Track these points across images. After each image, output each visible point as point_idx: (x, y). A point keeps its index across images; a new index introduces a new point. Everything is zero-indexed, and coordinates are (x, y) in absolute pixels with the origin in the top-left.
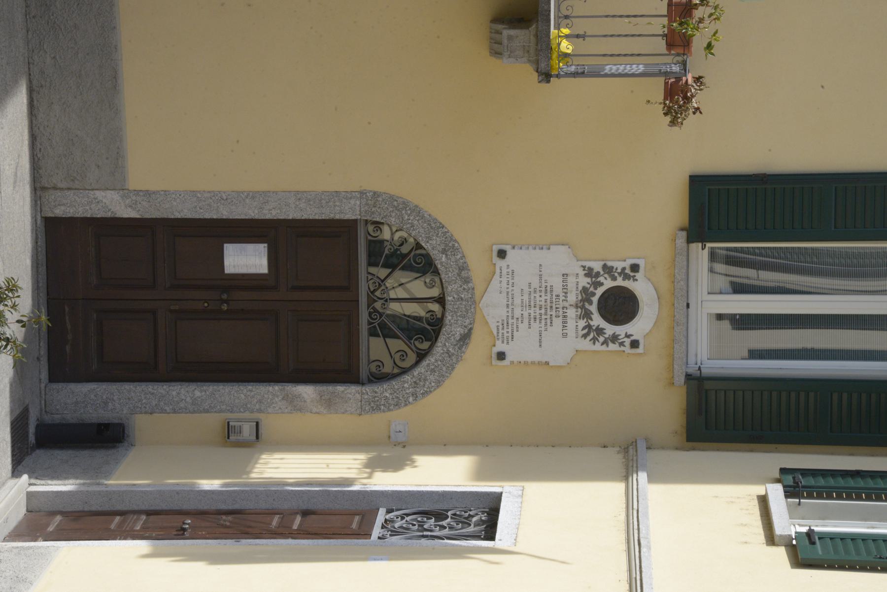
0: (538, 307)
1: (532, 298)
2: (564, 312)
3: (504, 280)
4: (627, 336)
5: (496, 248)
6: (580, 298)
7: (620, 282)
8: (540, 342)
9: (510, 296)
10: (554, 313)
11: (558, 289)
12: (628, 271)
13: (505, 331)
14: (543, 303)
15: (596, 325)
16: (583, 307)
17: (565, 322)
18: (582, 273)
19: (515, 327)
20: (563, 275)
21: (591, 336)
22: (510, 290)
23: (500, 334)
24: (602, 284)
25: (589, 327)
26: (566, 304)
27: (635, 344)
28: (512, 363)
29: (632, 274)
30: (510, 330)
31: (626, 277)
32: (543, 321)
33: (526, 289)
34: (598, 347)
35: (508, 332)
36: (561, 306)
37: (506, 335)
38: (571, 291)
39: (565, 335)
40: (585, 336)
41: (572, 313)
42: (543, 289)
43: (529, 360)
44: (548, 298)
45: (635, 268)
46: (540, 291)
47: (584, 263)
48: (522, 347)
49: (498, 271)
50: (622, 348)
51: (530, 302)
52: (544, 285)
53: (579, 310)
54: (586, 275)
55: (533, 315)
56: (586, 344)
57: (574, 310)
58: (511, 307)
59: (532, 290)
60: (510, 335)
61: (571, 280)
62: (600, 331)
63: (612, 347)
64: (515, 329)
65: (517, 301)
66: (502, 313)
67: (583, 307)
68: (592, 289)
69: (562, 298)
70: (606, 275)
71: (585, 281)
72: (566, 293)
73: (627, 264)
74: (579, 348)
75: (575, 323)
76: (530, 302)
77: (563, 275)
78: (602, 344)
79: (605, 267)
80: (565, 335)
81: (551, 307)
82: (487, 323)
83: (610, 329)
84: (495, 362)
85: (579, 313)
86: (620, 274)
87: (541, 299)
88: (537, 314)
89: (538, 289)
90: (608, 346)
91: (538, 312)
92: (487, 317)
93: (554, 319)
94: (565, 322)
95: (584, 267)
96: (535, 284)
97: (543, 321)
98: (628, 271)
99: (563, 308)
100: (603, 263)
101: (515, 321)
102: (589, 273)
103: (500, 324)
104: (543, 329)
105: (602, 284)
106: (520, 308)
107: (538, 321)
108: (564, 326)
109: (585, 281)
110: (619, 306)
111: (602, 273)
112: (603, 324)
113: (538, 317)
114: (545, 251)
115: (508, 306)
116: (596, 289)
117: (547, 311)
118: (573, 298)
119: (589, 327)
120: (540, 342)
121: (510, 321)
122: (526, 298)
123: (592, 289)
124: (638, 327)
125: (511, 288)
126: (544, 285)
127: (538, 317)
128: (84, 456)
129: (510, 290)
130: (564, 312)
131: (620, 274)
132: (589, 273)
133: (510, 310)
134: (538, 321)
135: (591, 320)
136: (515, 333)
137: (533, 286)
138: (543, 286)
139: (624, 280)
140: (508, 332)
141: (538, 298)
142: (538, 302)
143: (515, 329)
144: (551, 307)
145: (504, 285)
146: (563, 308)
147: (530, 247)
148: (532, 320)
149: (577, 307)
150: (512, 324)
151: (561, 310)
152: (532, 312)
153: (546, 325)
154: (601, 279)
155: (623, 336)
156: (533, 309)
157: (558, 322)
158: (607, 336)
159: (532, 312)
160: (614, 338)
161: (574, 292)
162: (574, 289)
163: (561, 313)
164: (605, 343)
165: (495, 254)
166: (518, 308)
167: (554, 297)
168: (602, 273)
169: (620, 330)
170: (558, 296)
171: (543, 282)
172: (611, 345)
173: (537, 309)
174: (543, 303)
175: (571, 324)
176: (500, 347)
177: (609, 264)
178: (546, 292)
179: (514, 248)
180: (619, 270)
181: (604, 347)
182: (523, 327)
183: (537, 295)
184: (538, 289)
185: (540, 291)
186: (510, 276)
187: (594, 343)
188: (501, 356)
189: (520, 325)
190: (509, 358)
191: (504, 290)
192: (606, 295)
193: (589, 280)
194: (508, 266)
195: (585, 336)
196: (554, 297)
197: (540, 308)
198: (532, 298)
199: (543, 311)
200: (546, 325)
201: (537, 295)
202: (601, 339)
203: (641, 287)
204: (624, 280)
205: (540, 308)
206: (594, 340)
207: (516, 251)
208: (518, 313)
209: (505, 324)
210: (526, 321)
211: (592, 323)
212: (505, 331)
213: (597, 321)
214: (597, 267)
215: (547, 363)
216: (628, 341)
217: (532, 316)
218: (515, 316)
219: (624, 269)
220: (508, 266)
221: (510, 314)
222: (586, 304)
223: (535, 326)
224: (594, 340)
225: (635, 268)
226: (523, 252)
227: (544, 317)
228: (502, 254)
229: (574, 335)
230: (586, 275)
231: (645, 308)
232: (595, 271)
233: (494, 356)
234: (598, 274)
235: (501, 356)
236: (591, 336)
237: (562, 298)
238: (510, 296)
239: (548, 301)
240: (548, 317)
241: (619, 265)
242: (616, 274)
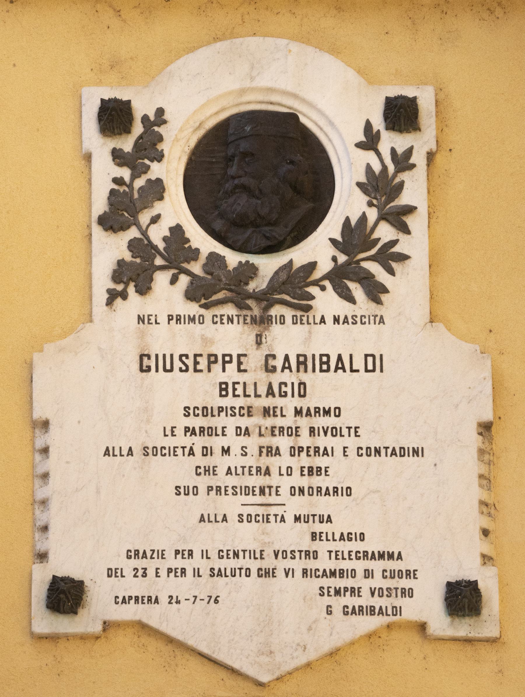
0: (265, 461)
1: (232, 481)
2: (286, 366)
3: (167, 586)
4: (370, 141)
5: (45, 622)
6: (230, 310)
7: (171, 170)
8: (403, 452)
9: (230, 564)
10: (290, 404)
11: (201, 388)
12: (127, 144)
13: (366, 585)
14: (253, 443)
15: (332, 251)
16: (266, 298)
17: (324, 364)
18: (134, 303)
19: (346, 547)
20: (144, 369)
21: (375, 268)
22: (204, 566)
23: (377, 602)
24: (177, 231)
25: (339, 277)
26: (255, 359)
27: (401, 114)
28: (486, 559)
29: (138, 129)
30: (360, 566)
31: (149, 147)
32: (322, 441)
33: (201, 504)
34: (415, 244)
35: (368, 574)
36: (264, 379)
37: (378, 582)
38: (206, 341)
39: (374, 363)
40: (376, 291)
41: (287, 337)
42: (199, 442)
43: (476, 493)
44: (231, 423)
45: (114, 116)
46: (206, 451)
47: (100, 296)
48: (426, 520)
49: (130, 612)
50: (418, 158)
51: (248, 491)
52: (182, 440)
53: (276, 311)
54: (144, 290)
55: (297, 480)
56: (407, 286)
57: (276, 329)
58: (269, 562)
59: (203, 482)
60: (377, 566)
61: (165, 340)
62: (354, 238)
63: (414, 190)
64: (355, 546)
65: (246, 536)
66: (293, 598)
67: (266, 298)
68: (196, 268)
69: (231, 374)
70: (144, 218)
71: (167, 294)
72: (212, 359)
73: (100, 147)
74: (420, 310)
75: (330, 324)
76: (248, 491)
77: (144, 369)
78: (405, 229)
79: (111, 222)
80: (374, 363)
81: (266, 412)
82: (333, 654)
83: (348, 202)
84: (487, 626)
85: (288, 313)
86: (138, 171)
87: (238, 449)
88: (295, 463)
89: (199, 460)
90: (410, 210)
91: (285, 460)
92: (312, 655)
93: (310, 402)
94: (324, 364)
95: (113, 296)
96: (181, 470)
97: (322, 441)
98: (127, 144)
99: (270, 370)
100: (97, 231)
101: (322, 547)
102: (134, 276)
103: (338, 603)
104: (352, 442)
105: (177, 231)
106: (273, 526)
107: (321, 462)
108: (340, 366)
109: (167, 294)
110: (261, 177)
111: (133, 233)
112: (331, 227)
113: (305, 461)
114: (54, 438)
115: (266, 573)
116: (195, 254)
117: (284, 432)
118: (230, 335)
119: (339, 277)
120: (403, 452)
121: (324, 563)
122: (232, 505)
123: (196, 268)
124: (336, 107)
125: (197, 561)
126: (182, 440)
127: (305, 461)
128: (468, 638)
129: (204, 566)
130: (286, 366)
131: (138, 171)
132: (134, 276)
133: (282, 564)
134: (321, 462)
135: (312, 266)
136: (371, 545)
137: (189, 480)
138: (188, 441)
139: (159, 157)
140: (368, 574)
141: (235, 460)
142: (250, 461)
143: (355, 546)
144: (266, 412)
145: (183, 587)
146: (270, 370)
147: (42, 518)
148: (317, 481)
149: (264, 321)
150: (337, 555)
151: (276, 379)
152: (286, 483)
153: (335, 432)
154: (157, 235)
155: (370, 157)
156: (274, 480)
157: (323, 389)
158: (372, 215)
159: (286, 483)
160: (380, 187)
161: (208, 329)
162: (196, 328)
163: (287, 377)
164: (399, 218)
165: (63, 624)
166: (262, 396)
167: (228, 402)
168: (133, 233)
169: (349, 167)
170: (223, 389)
171: (169, 442)
172: (405, 199)
173: (274, 462)
174: (253, 443)
175: (328, 340)
176: (427, 604)
177: (100, 205)
178: (211, 431)
179: (42, 557)
180: (125, 173)
181: (417, 223)
182: (344, 516)
183: (222, 463)
184: (199, 460)
185: (206, 451)
186: (151, 565)
187: (403, 258)
188: (462, 598)
189: (338, 527)
190: (470, 570)
191: (206, 586)
192: (218, 225)
193: (162, 279)
194: (111, 573)
195: (376, 291)
196: (228, 402)
197: (273, 451)
198: (232, 481)
199: (284, 443)
200: (335, 432)
201: (222, 463)
202: (385, 232)
203: (193, 95)
204: (159, 157)
205: (273, 451)
206: (389, 257)
207: (53, 543)
208: (294, 536)
209: (335, 583)
210: (323, 505)
211: (325, 266)
212: (366, 585)
213: (318, 249)
214: (112, 249)
215: (485, 428)
216: (389, 141)
217: (305, 482)
218: (306, 544)
219: (117, 156)
220: (111, 573)
221: (298, 565)
222: (252, 286)
223: (340, 470)
224: (389, 257)
225: (114, 116)
226: (55, 517)
227: (305, 440)
228: (65, 596)
229: (372, 328)
230: (144, 290)
231: (263, 82)
232: (127, 256)
233: (464, 628)
234: (141, 247)
235: (462, 598)
236: (375, 268)
237: (231, 374)
238: (230, 564)
239: (244, 422)
240: (304, 423)
241: (105, 172)
242: (139, 183)
